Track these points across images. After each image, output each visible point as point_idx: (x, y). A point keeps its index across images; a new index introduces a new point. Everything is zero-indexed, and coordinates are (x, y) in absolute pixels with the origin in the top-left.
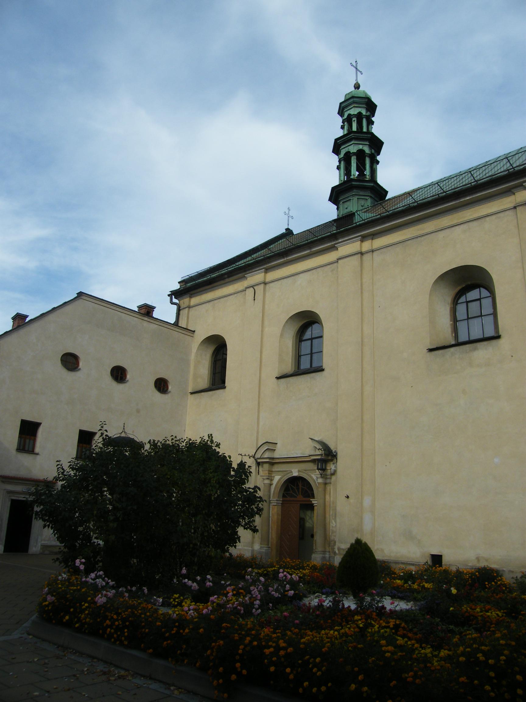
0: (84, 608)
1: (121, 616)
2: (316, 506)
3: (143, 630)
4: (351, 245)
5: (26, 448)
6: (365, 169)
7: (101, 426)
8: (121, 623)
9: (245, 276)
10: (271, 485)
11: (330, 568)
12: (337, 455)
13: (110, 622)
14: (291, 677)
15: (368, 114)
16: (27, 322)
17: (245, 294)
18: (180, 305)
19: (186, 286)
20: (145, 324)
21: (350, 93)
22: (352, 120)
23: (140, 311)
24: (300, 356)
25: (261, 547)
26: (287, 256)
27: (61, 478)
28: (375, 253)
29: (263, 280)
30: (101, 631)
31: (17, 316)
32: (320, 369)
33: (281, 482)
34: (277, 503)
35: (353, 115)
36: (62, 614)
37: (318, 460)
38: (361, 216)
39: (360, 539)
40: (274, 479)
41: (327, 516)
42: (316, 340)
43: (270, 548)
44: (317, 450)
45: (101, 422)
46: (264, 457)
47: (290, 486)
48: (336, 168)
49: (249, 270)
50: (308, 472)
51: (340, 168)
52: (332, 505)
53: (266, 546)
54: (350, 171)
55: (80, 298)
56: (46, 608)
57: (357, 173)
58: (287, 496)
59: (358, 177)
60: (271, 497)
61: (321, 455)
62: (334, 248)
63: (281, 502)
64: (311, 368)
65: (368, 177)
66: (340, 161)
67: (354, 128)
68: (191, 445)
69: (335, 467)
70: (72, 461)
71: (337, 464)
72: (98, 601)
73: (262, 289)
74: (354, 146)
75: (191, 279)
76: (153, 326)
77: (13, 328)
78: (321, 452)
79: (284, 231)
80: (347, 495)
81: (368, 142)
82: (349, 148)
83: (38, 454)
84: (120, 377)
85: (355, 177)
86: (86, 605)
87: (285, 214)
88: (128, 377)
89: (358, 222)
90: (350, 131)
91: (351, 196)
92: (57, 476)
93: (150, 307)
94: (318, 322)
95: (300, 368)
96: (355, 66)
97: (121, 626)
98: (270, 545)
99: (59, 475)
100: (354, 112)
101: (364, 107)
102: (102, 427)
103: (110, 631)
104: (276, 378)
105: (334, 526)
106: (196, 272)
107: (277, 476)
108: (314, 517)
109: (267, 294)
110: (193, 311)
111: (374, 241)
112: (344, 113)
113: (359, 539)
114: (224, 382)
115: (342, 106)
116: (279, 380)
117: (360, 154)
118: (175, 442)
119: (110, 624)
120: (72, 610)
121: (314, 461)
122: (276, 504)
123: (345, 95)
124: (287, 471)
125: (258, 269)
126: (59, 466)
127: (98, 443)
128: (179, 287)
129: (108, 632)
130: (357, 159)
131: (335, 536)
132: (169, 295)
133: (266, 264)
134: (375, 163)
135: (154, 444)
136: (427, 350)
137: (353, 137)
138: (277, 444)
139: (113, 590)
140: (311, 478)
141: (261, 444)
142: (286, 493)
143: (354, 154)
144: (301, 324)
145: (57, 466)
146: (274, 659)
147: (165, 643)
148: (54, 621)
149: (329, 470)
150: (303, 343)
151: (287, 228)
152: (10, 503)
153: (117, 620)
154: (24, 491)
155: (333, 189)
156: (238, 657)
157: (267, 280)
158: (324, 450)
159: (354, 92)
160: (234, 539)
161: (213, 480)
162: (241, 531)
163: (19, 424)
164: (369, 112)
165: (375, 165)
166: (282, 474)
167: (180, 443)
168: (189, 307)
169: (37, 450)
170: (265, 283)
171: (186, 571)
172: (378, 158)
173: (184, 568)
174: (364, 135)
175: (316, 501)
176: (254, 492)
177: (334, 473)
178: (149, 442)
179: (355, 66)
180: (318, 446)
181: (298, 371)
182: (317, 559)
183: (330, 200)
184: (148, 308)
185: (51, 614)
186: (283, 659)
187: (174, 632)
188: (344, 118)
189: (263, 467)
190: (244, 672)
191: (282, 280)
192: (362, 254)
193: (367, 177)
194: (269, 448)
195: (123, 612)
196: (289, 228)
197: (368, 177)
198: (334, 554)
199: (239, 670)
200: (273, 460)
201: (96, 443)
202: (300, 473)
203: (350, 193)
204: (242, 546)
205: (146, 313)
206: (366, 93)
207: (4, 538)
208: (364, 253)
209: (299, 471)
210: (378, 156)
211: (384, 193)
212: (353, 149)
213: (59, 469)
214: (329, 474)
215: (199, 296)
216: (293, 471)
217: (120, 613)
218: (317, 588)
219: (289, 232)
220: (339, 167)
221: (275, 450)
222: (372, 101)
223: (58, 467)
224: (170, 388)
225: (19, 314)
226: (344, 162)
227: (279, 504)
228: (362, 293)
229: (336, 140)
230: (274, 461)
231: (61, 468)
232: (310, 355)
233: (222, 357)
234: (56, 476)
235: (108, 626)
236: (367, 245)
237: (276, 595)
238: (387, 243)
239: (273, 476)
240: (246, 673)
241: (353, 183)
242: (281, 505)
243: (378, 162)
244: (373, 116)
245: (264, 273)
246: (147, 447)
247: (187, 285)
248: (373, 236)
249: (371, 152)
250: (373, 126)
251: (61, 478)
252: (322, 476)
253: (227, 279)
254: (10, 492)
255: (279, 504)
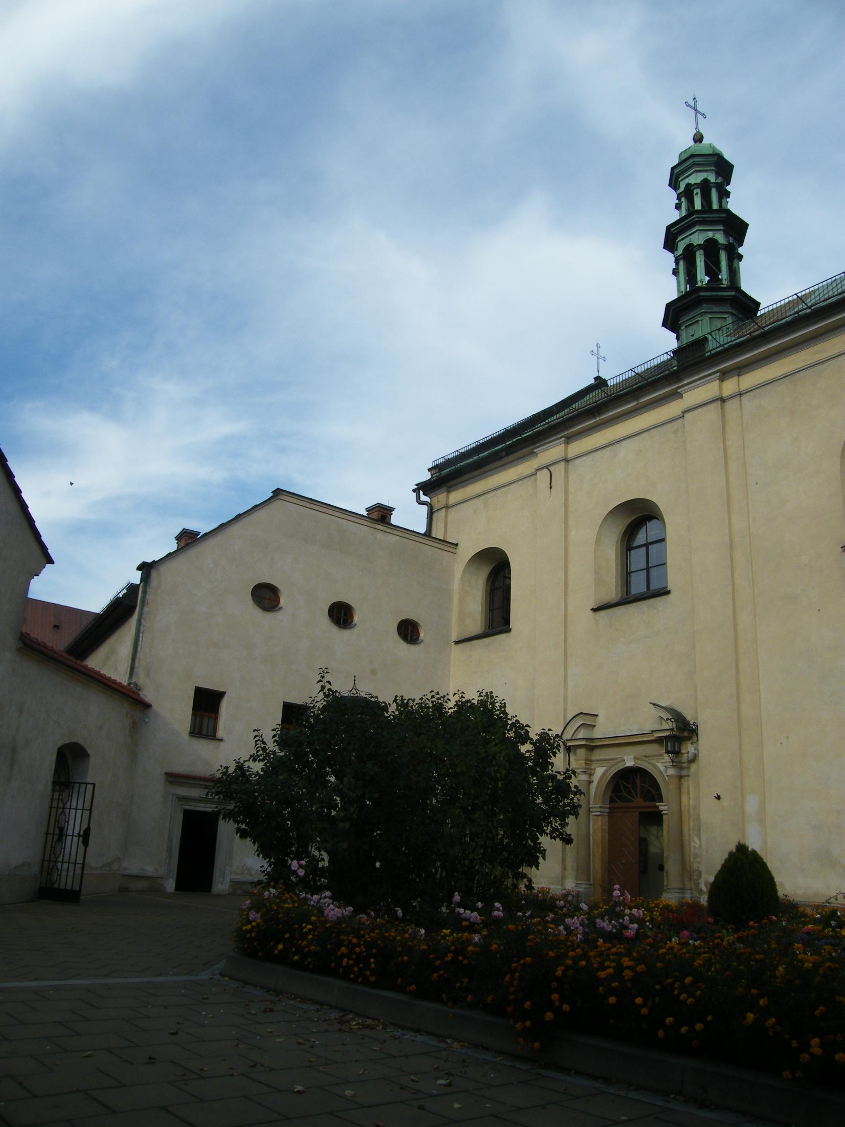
0: (306, 932)
1: (363, 939)
2: (667, 814)
3: (400, 959)
4: (704, 388)
5: (204, 732)
6: (720, 271)
7: (321, 675)
8: (364, 949)
9: (535, 451)
10: (590, 782)
11: (694, 907)
12: (698, 729)
13: (347, 950)
14: (645, 1011)
15: (720, 180)
16: (199, 538)
17: (536, 480)
18: (432, 505)
19: (440, 474)
20: (380, 535)
21: (686, 150)
22: (693, 192)
23: (370, 516)
24: (631, 572)
25: (577, 884)
26: (600, 414)
27: (261, 757)
28: (744, 398)
29: (564, 455)
30: (333, 965)
31: (183, 534)
32: (664, 592)
33: (607, 778)
34: (600, 812)
35: (695, 184)
36: (272, 943)
37: (666, 737)
38: (718, 340)
39: (745, 844)
40: (595, 774)
41: (685, 830)
42: (655, 546)
43: (592, 886)
44: (664, 723)
45: (321, 668)
46: (578, 738)
47: (622, 784)
48: (672, 273)
49: (540, 441)
50: (650, 760)
51: (678, 272)
52: (692, 812)
53: (586, 882)
54: (695, 276)
55: (278, 497)
56: (249, 935)
57: (707, 279)
58: (618, 800)
59: (708, 283)
60: (591, 803)
61: (672, 729)
62: (676, 395)
63: (607, 810)
64: (648, 592)
65: (725, 283)
66: (677, 262)
67: (698, 205)
68: (463, 706)
69: (696, 749)
70: (277, 728)
71: (697, 744)
72: (328, 916)
73: (563, 470)
74: (700, 235)
75: (448, 463)
76: (392, 539)
77: (180, 547)
78: (670, 723)
79: (593, 381)
80: (717, 794)
81: (722, 226)
82: (690, 239)
83: (221, 740)
84: (344, 619)
85: (704, 283)
86: (309, 927)
87: (593, 354)
88: (356, 619)
89: (712, 350)
90: (691, 211)
91: (698, 315)
92: (256, 754)
93: (387, 509)
94: (658, 518)
95: (630, 592)
96: (693, 106)
97: (365, 954)
98: (592, 881)
99: (258, 752)
100: (696, 181)
101: (711, 170)
102: (323, 677)
103: (348, 963)
104: (591, 610)
105: (697, 846)
106: (455, 452)
107: (598, 768)
108: (662, 835)
109: (570, 478)
110: (452, 513)
111: (742, 378)
112: (679, 184)
113: (743, 844)
114: (507, 622)
115: (675, 172)
116: (598, 613)
117: (710, 247)
118: (437, 701)
119: (347, 952)
120: (287, 935)
121: (659, 741)
122: (599, 813)
123: (680, 155)
124: (617, 759)
125: (554, 438)
126: (257, 738)
127: (317, 702)
128: (429, 477)
129: (344, 964)
130: (706, 255)
131: (699, 863)
132: (414, 491)
133: (567, 429)
134: (736, 259)
135: (403, 704)
136: (842, 548)
137: (696, 219)
138: (597, 715)
139: (349, 906)
140: (656, 768)
141: (573, 716)
142: (614, 796)
143: (700, 247)
144: (628, 521)
145: (254, 738)
146: (615, 984)
147: (435, 975)
148: (260, 954)
149: (686, 755)
150: (632, 552)
151: (597, 375)
152: (181, 815)
153: (359, 945)
154: (202, 796)
155: (669, 306)
156: (554, 984)
157: (570, 456)
158: (676, 721)
159: (695, 147)
160: (533, 856)
161: (500, 756)
162: (545, 841)
163: (194, 688)
164: (720, 178)
165: (736, 261)
166: (608, 765)
167: (445, 701)
168: (447, 507)
169: (220, 734)
170: (567, 460)
171: (459, 898)
172: (741, 250)
173: (457, 893)
174: (714, 215)
175: (666, 805)
176: (565, 778)
177: (694, 759)
178: (395, 700)
179: (693, 106)
180: (666, 715)
181: (628, 598)
182: (670, 898)
183: (664, 325)
184: (382, 510)
185: (256, 943)
186: (629, 985)
187: (450, 958)
188: (679, 192)
189: (575, 754)
190: (566, 1007)
191: (594, 454)
192: (723, 400)
193: (724, 282)
194: (585, 722)
195: (366, 934)
196: (600, 375)
197: (725, 283)
198: (699, 894)
199: (557, 1004)
200: (592, 742)
201: (312, 702)
202: (637, 761)
203: (696, 311)
204: (545, 883)
205: (380, 518)
206: (714, 146)
207: (176, 869)
208: (727, 399)
209: (635, 758)
210: (739, 247)
211: (753, 306)
212: (698, 239)
213: (257, 743)
214: (686, 760)
215: (461, 488)
216: (625, 758)
217: (363, 936)
218: (674, 933)
219: (600, 382)
220: (676, 270)
221: (595, 726)
222: (725, 159)
223: (256, 739)
224: (422, 635)
225: (187, 531)
226: (683, 262)
227: (604, 814)
228: (726, 463)
229: (669, 228)
230: (594, 744)
231: (260, 741)
232: (645, 571)
233: (504, 582)
234: (254, 754)
235: (344, 956)
236: (730, 386)
237: (608, 928)
238: (764, 380)
239: (592, 767)
240: (568, 1009)
241: (702, 294)
242: (609, 816)
243: (740, 257)
244: (728, 184)
245: (564, 445)
246: (393, 708)
247: (441, 472)
248: (740, 370)
249: (728, 241)
250: (728, 200)
251: (261, 757)
252: (674, 764)
253: (505, 458)
254: (181, 799)
255: (604, 814)
